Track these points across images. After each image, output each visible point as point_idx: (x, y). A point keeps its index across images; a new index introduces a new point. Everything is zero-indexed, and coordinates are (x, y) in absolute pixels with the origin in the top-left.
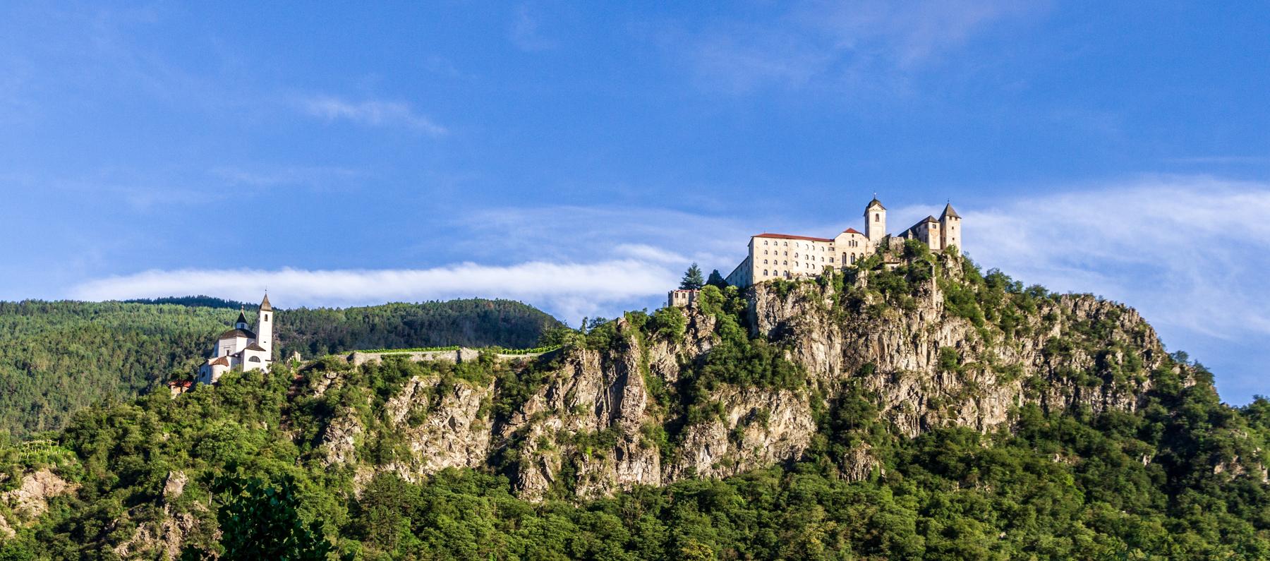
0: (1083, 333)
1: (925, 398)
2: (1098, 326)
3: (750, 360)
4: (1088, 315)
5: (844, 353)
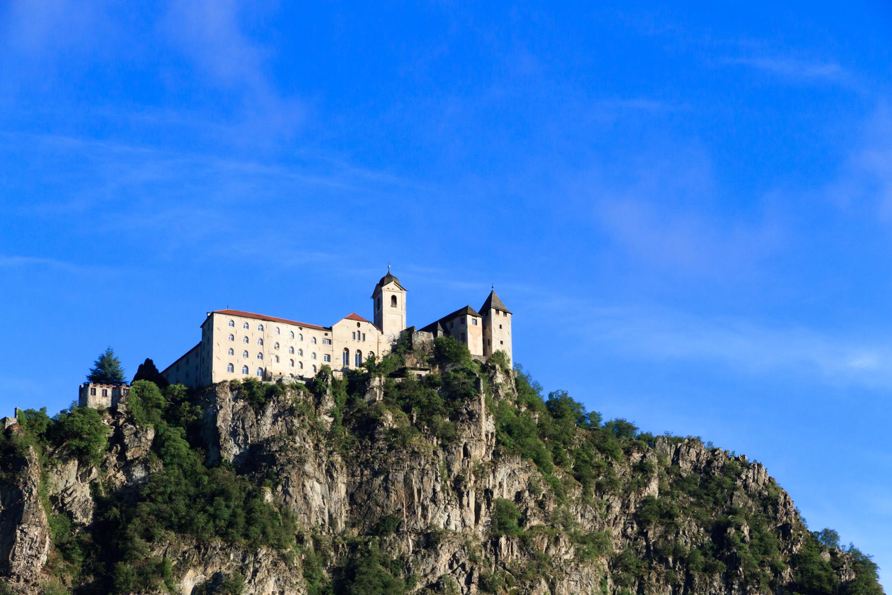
0: (691, 494)
1: (476, 575)
2: (713, 485)
3: (211, 498)
4: (695, 469)
5: (351, 497)
